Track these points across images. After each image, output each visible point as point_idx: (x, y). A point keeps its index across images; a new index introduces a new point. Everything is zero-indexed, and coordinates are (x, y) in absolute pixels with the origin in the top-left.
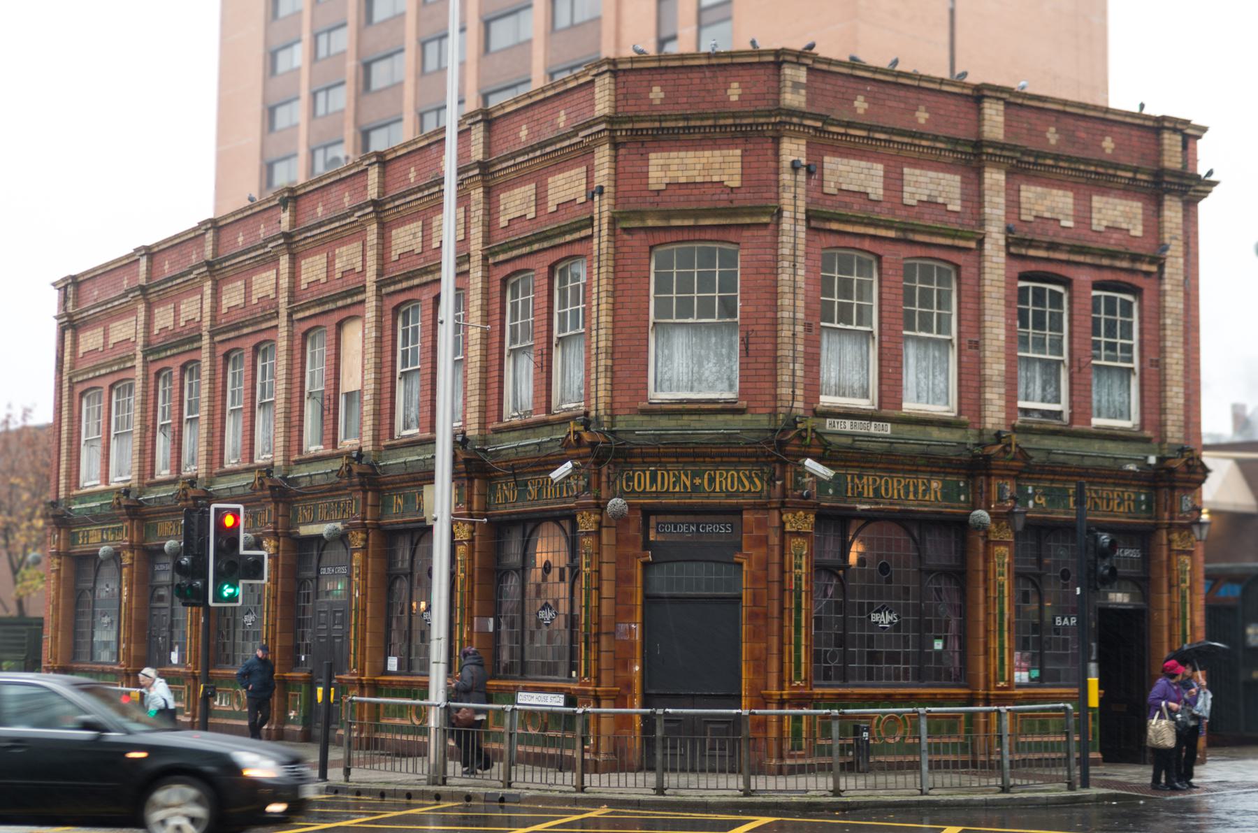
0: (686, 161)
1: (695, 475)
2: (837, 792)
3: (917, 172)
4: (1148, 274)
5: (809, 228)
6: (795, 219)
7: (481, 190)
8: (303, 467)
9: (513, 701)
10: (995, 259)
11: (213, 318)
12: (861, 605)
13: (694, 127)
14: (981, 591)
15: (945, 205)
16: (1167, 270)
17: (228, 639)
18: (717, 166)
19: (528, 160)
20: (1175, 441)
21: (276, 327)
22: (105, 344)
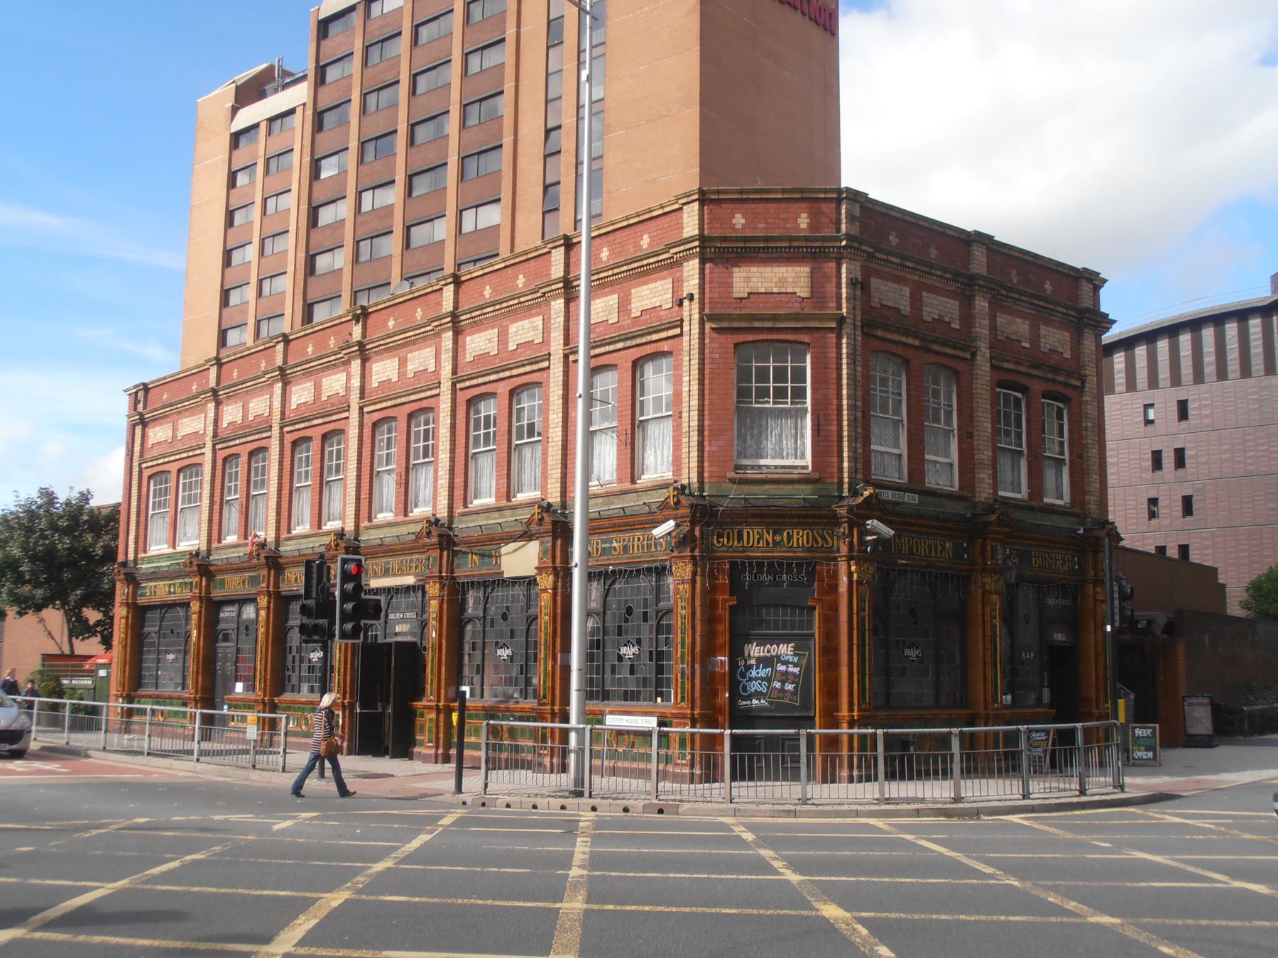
0: (764, 275)
1: (775, 533)
2: (958, 799)
3: (932, 296)
4: (1075, 387)
5: (863, 334)
6: (855, 326)
7: (563, 300)
8: (372, 531)
9: (601, 722)
10: (983, 368)
11: (283, 414)
12: (898, 641)
13: (772, 248)
14: (980, 631)
15: (949, 323)
16: (1087, 385)
17: (293, 672)
18: (791, 280)
19: (613, 275)
20: (1095, 516)
21: (270, 437)
22: (174, 436)
